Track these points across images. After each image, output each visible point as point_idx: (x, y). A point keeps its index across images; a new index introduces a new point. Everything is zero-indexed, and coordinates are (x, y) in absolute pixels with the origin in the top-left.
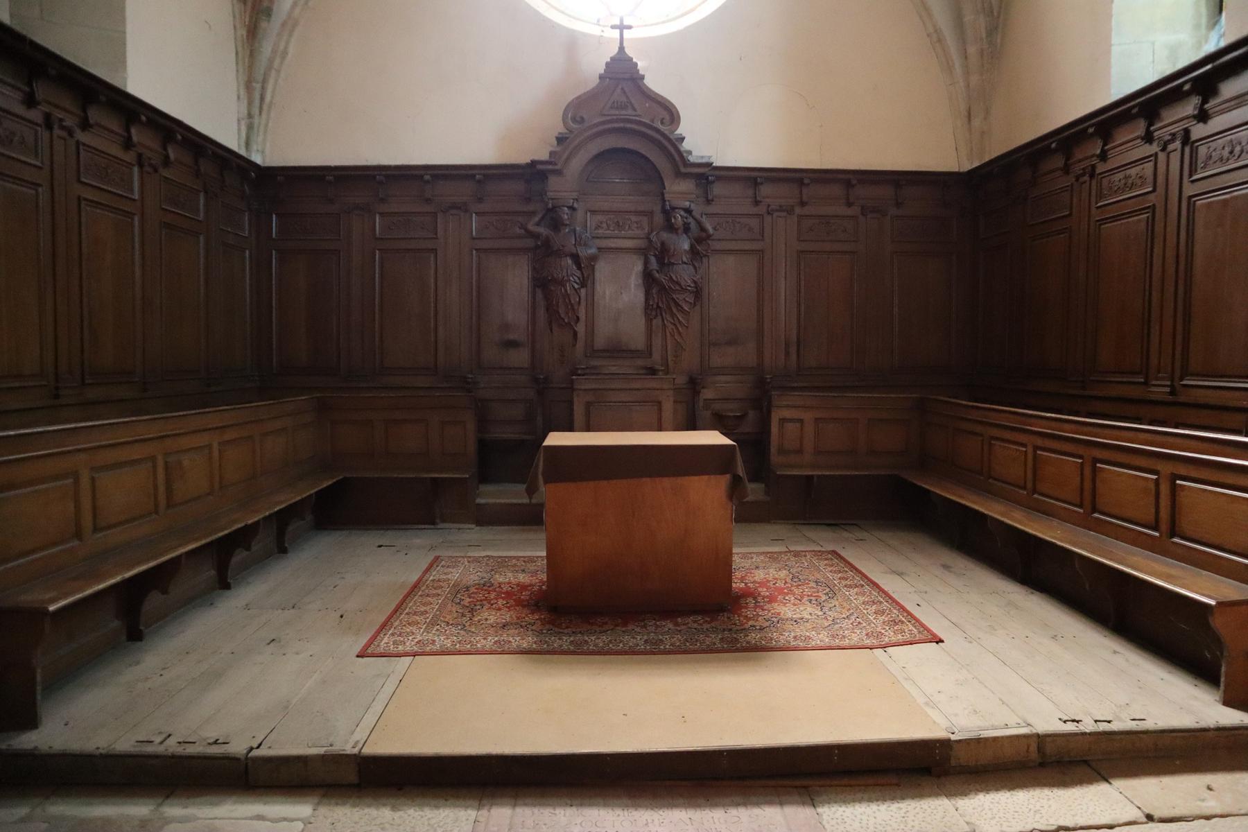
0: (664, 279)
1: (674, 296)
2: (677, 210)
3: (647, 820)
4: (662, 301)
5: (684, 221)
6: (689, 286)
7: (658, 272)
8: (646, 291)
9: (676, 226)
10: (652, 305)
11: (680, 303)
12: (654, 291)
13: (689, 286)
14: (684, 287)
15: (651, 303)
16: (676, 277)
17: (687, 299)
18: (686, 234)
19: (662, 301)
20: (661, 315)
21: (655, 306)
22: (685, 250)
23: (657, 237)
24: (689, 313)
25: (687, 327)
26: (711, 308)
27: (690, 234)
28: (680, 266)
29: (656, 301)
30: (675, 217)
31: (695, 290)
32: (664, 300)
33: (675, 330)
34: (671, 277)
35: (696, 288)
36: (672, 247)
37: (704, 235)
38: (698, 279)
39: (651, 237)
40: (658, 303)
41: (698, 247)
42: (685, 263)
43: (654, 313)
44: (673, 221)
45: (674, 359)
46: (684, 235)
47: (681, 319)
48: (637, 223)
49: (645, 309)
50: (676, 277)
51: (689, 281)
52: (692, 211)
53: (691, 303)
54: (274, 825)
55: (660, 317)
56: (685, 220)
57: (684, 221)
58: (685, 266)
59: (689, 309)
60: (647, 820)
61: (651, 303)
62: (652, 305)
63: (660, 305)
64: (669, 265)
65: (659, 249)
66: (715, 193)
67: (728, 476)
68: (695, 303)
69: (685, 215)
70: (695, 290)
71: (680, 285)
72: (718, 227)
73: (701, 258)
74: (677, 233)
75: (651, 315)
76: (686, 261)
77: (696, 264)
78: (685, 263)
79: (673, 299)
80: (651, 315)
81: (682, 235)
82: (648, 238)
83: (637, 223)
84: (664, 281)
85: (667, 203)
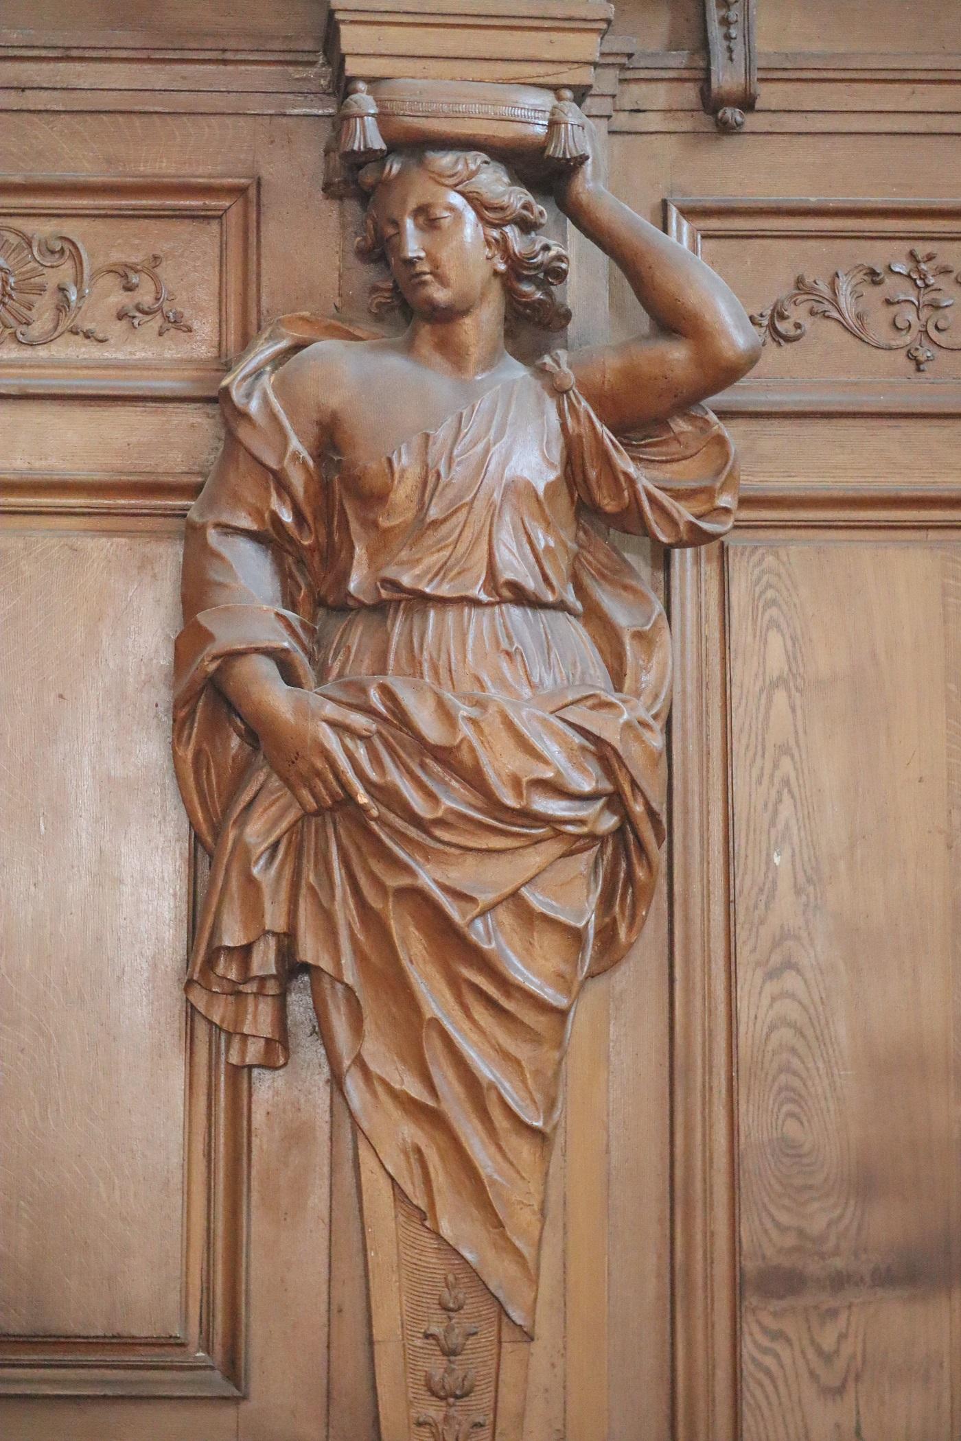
0: (339, 727)
1: (427, 877)
2: (445, 160)
3: (427, 1336)
4: (327, 918)
5: (502, 245)
6: (555, 789)
7: (290, 676)
8: (196, 839)
9: (440, 295)
10: (245, 952)
11: (478, 933)
12: (257, 833)
13: (555, 789)
14: (510, 801)
15: (232, 936)
16: (446, 714)
17: (536, 899)
18: (528, 356)
19: (327, 918)
20: (323, 1032)
21: (265, 960)
22: (519, 490)
23: (282, 388)
24: (562, 1014)
25: (541, 1137)
26: (748, 979)
27: (561, 361)
28: (478, 623)
29: (274, 918)
30: (428, 219)
31: (609, 822)
32: (344, 911)
33: (439, 1178)
34: (399, 718)
35: (615, 801)
36: (406, 461)
37: (678, 354)
38: (630, 729)
39: (235, 382)
40: (287, 941)
41: (624, 462)
42: (520, 597)
43: (259, 1021)
44: (413, 244)
45: (433, 1411)
46: (517, 372)
47: (486, 1070)
48: (124, 275)
49: (189, 985)
50: (446, 714)
51: (552, 749)
52: (571, 166)
53: (576, 936)
54: (463, 594)
55: (310, 1052)
56: (516, 241)
57: (502, 245)
58: (516, 613)
59: (562, 981)
60: (427, 1336)
61: (232, 936)
62: (245, 952)
63: (309, 949)
64: (380, 609)
65: (297, 480)
66: (761, 45)
67: (384, 147)
68: (607, 935)
69: (516, 197)
70: (609, 822)
71: (475, 779)
72: (798, 313)
73: (662, 558)
74: (452, 352)
75: (234, 1034)
76: (531, 584)
77: (621, 615)
78: (520, 597)
79: (416, 897)
80: (234, 1034)
81: (489, 363)
82: (222, 398)
83: (124, 275)
84: (332, 741)
85: (364, 100)
